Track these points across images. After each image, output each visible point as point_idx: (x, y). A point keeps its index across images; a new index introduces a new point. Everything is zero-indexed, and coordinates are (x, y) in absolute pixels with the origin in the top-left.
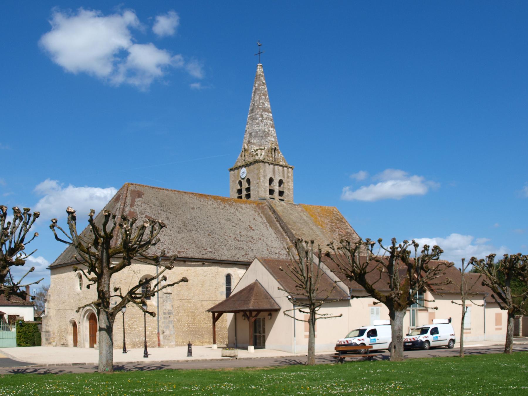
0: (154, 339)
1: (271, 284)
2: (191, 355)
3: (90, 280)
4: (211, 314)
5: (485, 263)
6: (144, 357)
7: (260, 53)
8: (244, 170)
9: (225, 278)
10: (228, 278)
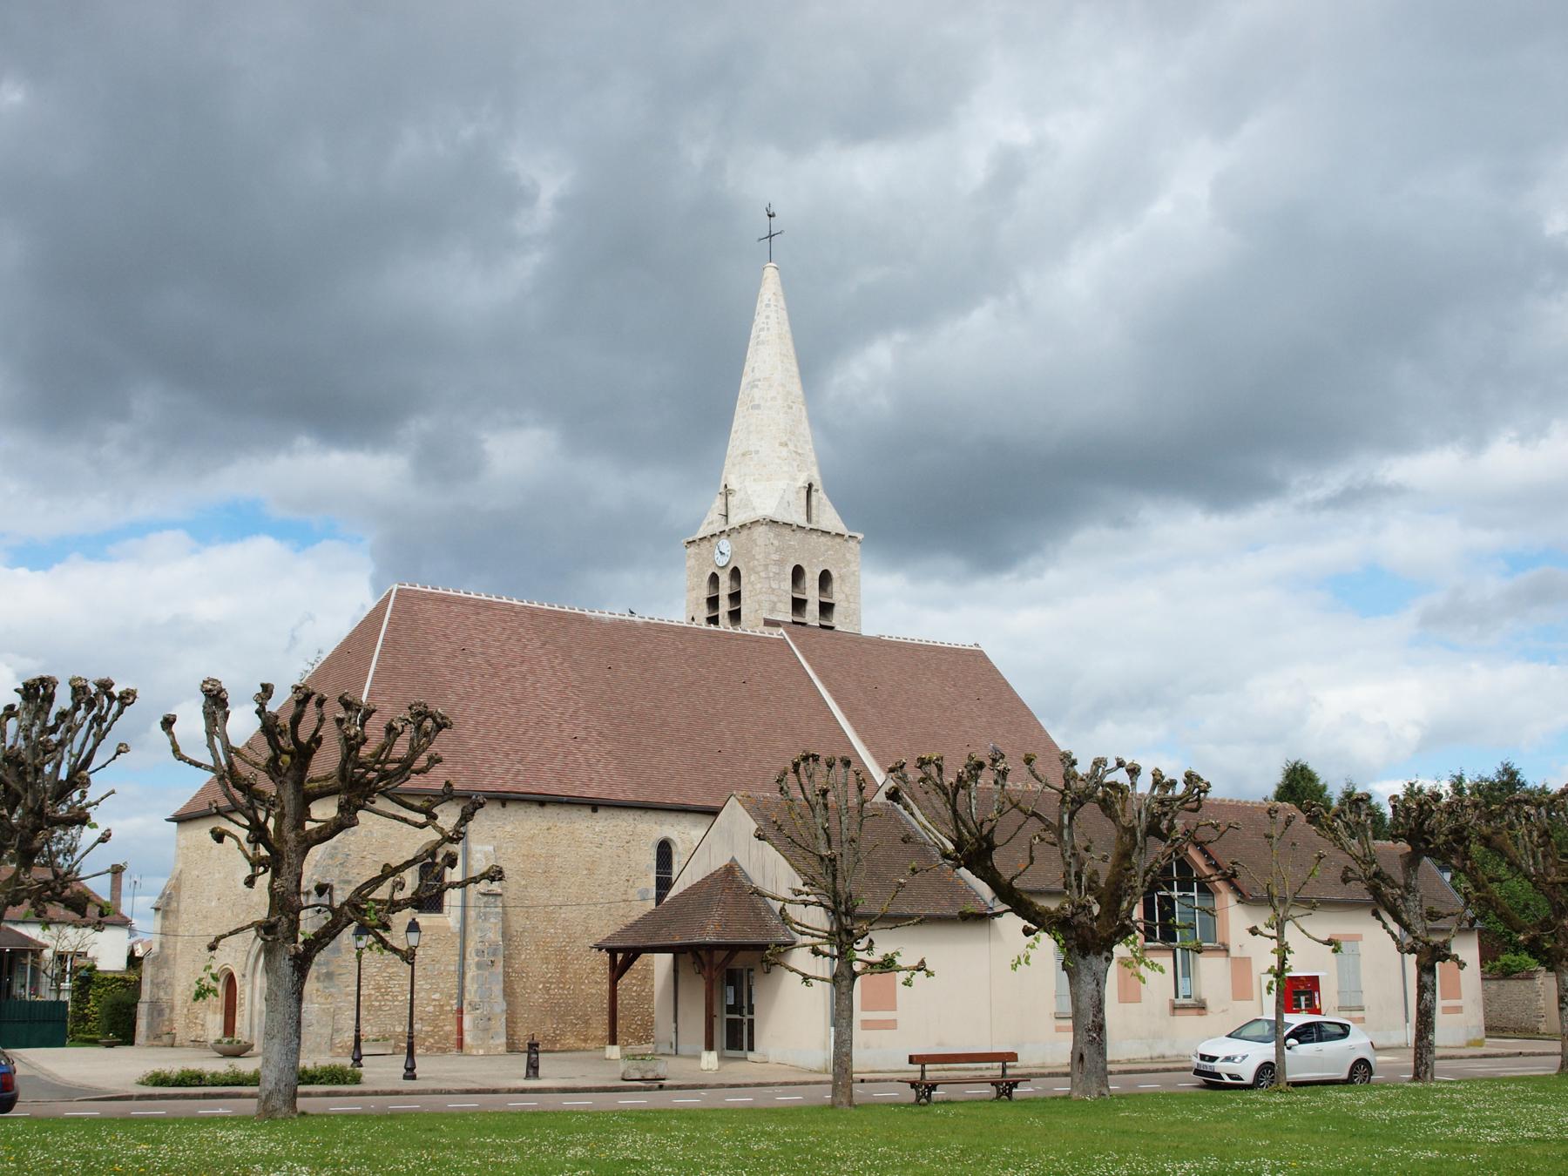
0: (447, 1028)
1: (774, 873)
2: (536, 1075)
4: (606, 956)
5: (1445, 800)
6: (405, 1077)
8: (725, 544)
9: (654, 852)
10: (664, 851)
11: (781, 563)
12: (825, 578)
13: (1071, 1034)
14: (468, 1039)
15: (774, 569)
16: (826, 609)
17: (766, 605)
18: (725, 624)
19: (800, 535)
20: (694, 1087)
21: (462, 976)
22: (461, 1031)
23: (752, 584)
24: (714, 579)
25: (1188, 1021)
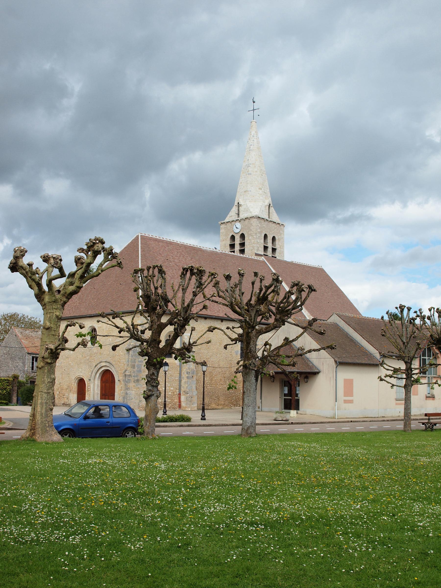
0: (176, 400)
3: (232, 341)
7: (254, 110)
8: (238, 225)
11: (260, 233)
12: (274, 239)
13: (404, 406)
14: (183, 404)
15: (258, 235)
16: (274, 250)
17: (256, 248)
18: (237, 253)
19: (266, 223)
20: (302, 423)
21: (180, 381)
22: (180, 402)
23: (250, 240)
24: (233, 238)
25: (430, 401)
